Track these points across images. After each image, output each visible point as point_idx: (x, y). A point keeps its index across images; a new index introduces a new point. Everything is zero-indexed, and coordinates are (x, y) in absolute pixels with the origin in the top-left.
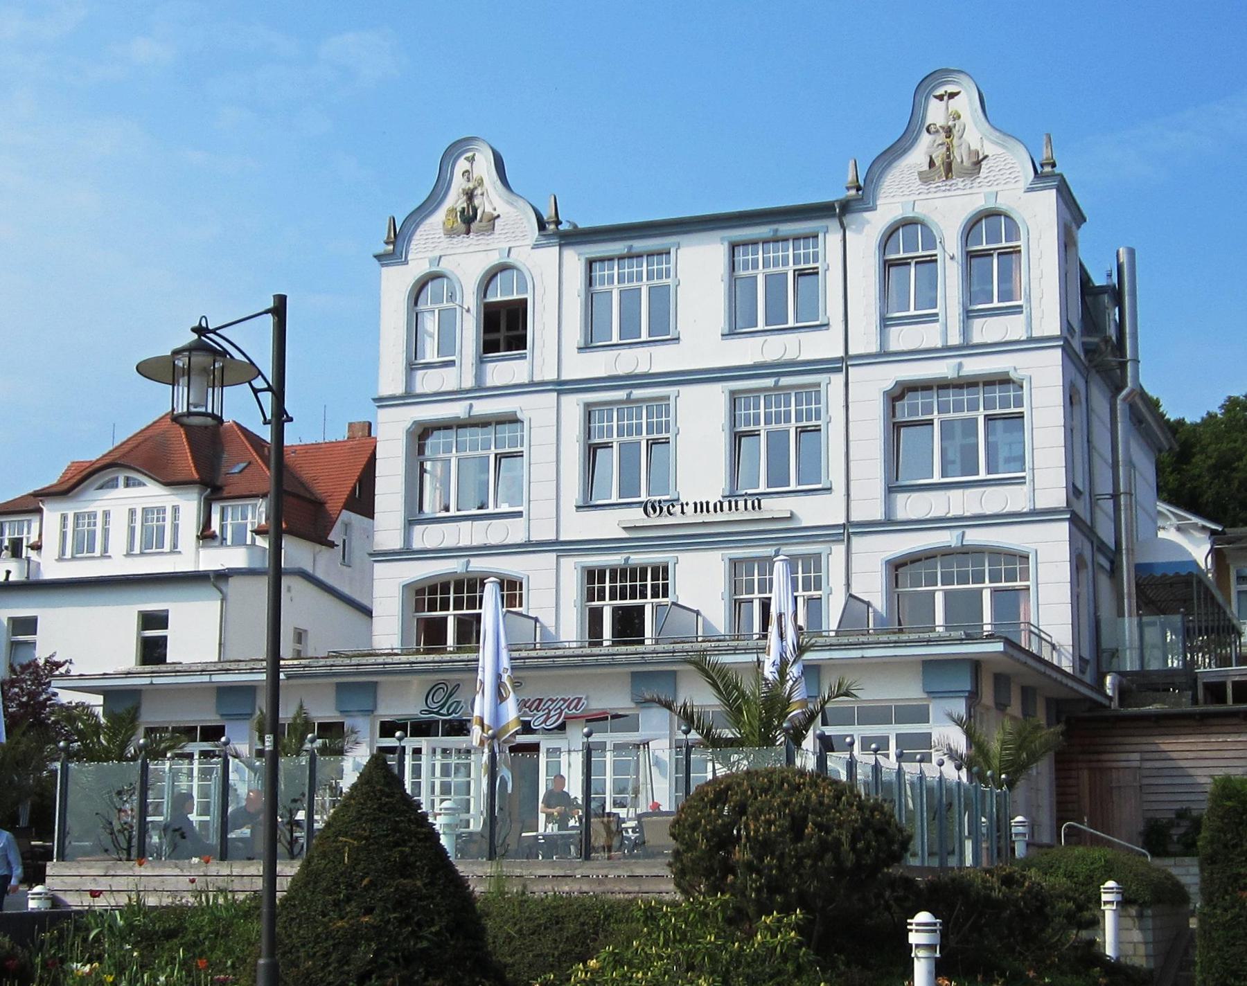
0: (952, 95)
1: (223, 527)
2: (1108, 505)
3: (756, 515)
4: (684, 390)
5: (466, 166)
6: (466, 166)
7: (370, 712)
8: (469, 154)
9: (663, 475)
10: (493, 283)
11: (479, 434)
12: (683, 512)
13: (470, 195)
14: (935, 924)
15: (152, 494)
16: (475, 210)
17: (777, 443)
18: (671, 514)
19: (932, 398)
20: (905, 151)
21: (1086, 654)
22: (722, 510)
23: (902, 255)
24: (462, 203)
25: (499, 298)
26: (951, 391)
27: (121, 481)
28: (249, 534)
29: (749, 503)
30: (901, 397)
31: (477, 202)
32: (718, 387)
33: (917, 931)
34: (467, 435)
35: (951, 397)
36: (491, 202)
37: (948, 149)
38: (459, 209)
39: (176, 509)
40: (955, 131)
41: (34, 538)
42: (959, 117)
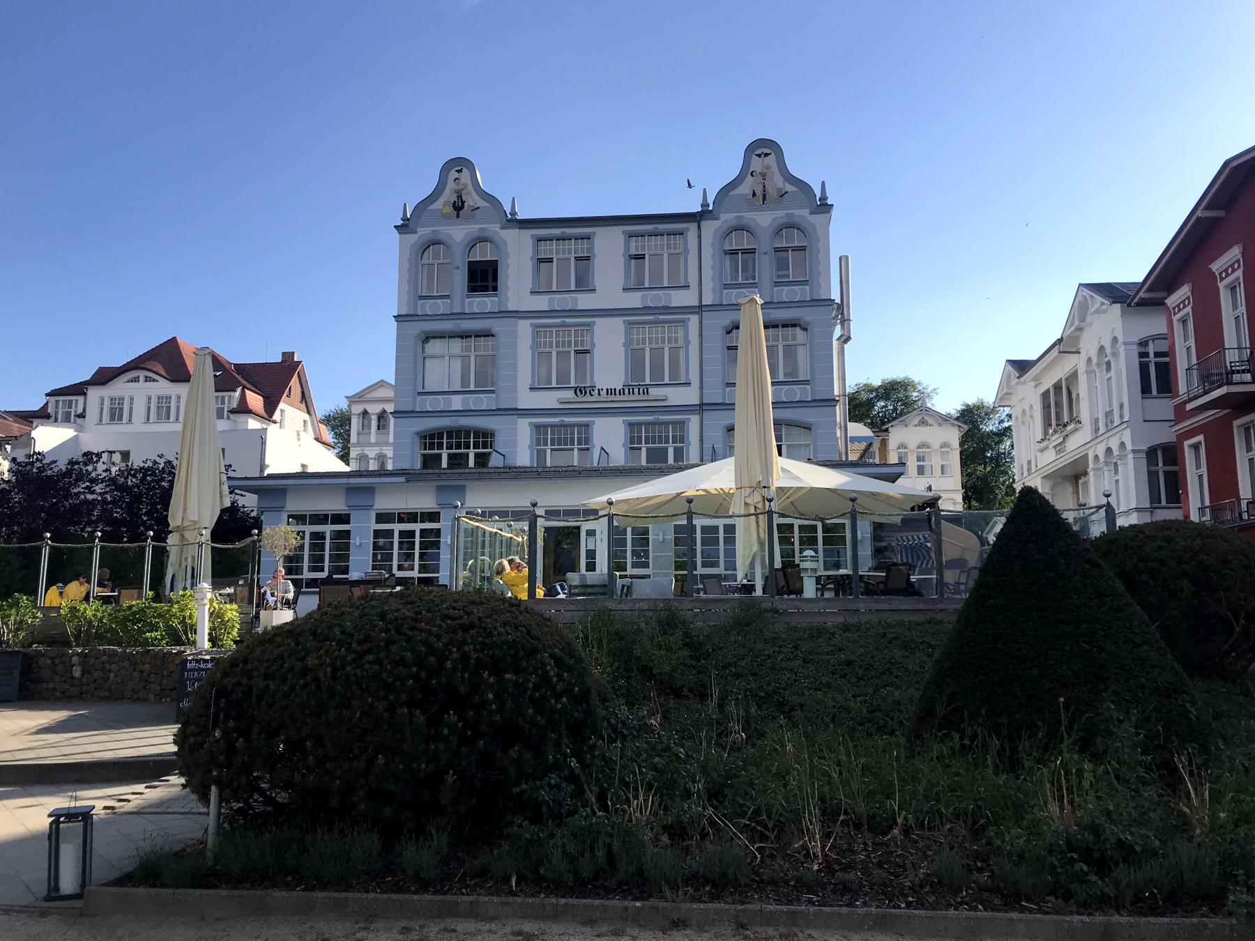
0: (766, 155)
3: (645, 397)
4: (598, 321)
7: (370, 507)
12: (599, 395)
16: (463, 202)
18: (592, 395)
20: (742, 183)
22: (624, 394)
25: (478, 259)
27: (142, 379)
29: (641, 390)
32: (620, 320)
40: (768, 175)
41: (80, 411)
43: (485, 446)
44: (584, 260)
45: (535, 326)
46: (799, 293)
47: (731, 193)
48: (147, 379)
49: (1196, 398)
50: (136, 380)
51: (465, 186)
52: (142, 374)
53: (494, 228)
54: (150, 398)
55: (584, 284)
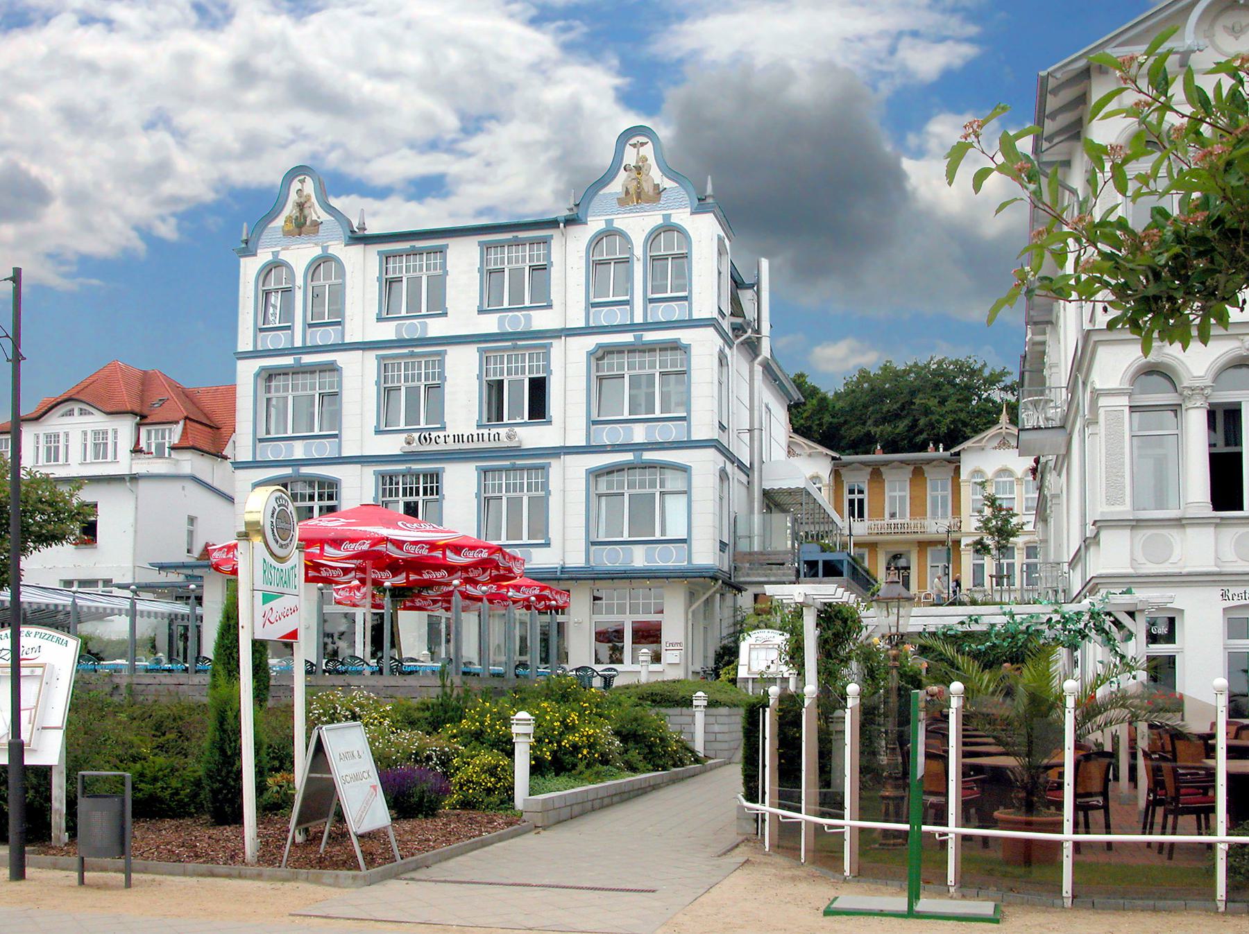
1: (149, 445)
2: (746, 437)
5: (299, 186)
6: (299, 186)
8: (302, 177)
9: (437, 413)
10: (317, 271)
11: (308, 379)
13: (301, 206)
14: (530, 720)
15: (97, 421)
16: (305, 218)
17: (412, 393)
19: (288, 381)
21: (726, 540)
23: (605, 257)
24: (295, 213)
26: (637, 354)
27: (76, 412)
28: (167, 450)
30: (602, 358)
31: (306, 212)
33: (517, 724)
34: (300, 380)
35: (637, 358)
36: (316, 213)
37: (639, 183)
38: (294, 217)
39: (116, 432)
40: (644, 170)
42: (647, 160)
43: (330, 497)
44: (541, 270)
45: (380, 358)
46: (331, 335)
47: (601, 192)
48: (82, 412)
49: (500, 470)
50: (71, 413)
51: (308, 197)
52: (76, 407)
53: (338, 249)
54: (85, 433)
55: (439, 309)
